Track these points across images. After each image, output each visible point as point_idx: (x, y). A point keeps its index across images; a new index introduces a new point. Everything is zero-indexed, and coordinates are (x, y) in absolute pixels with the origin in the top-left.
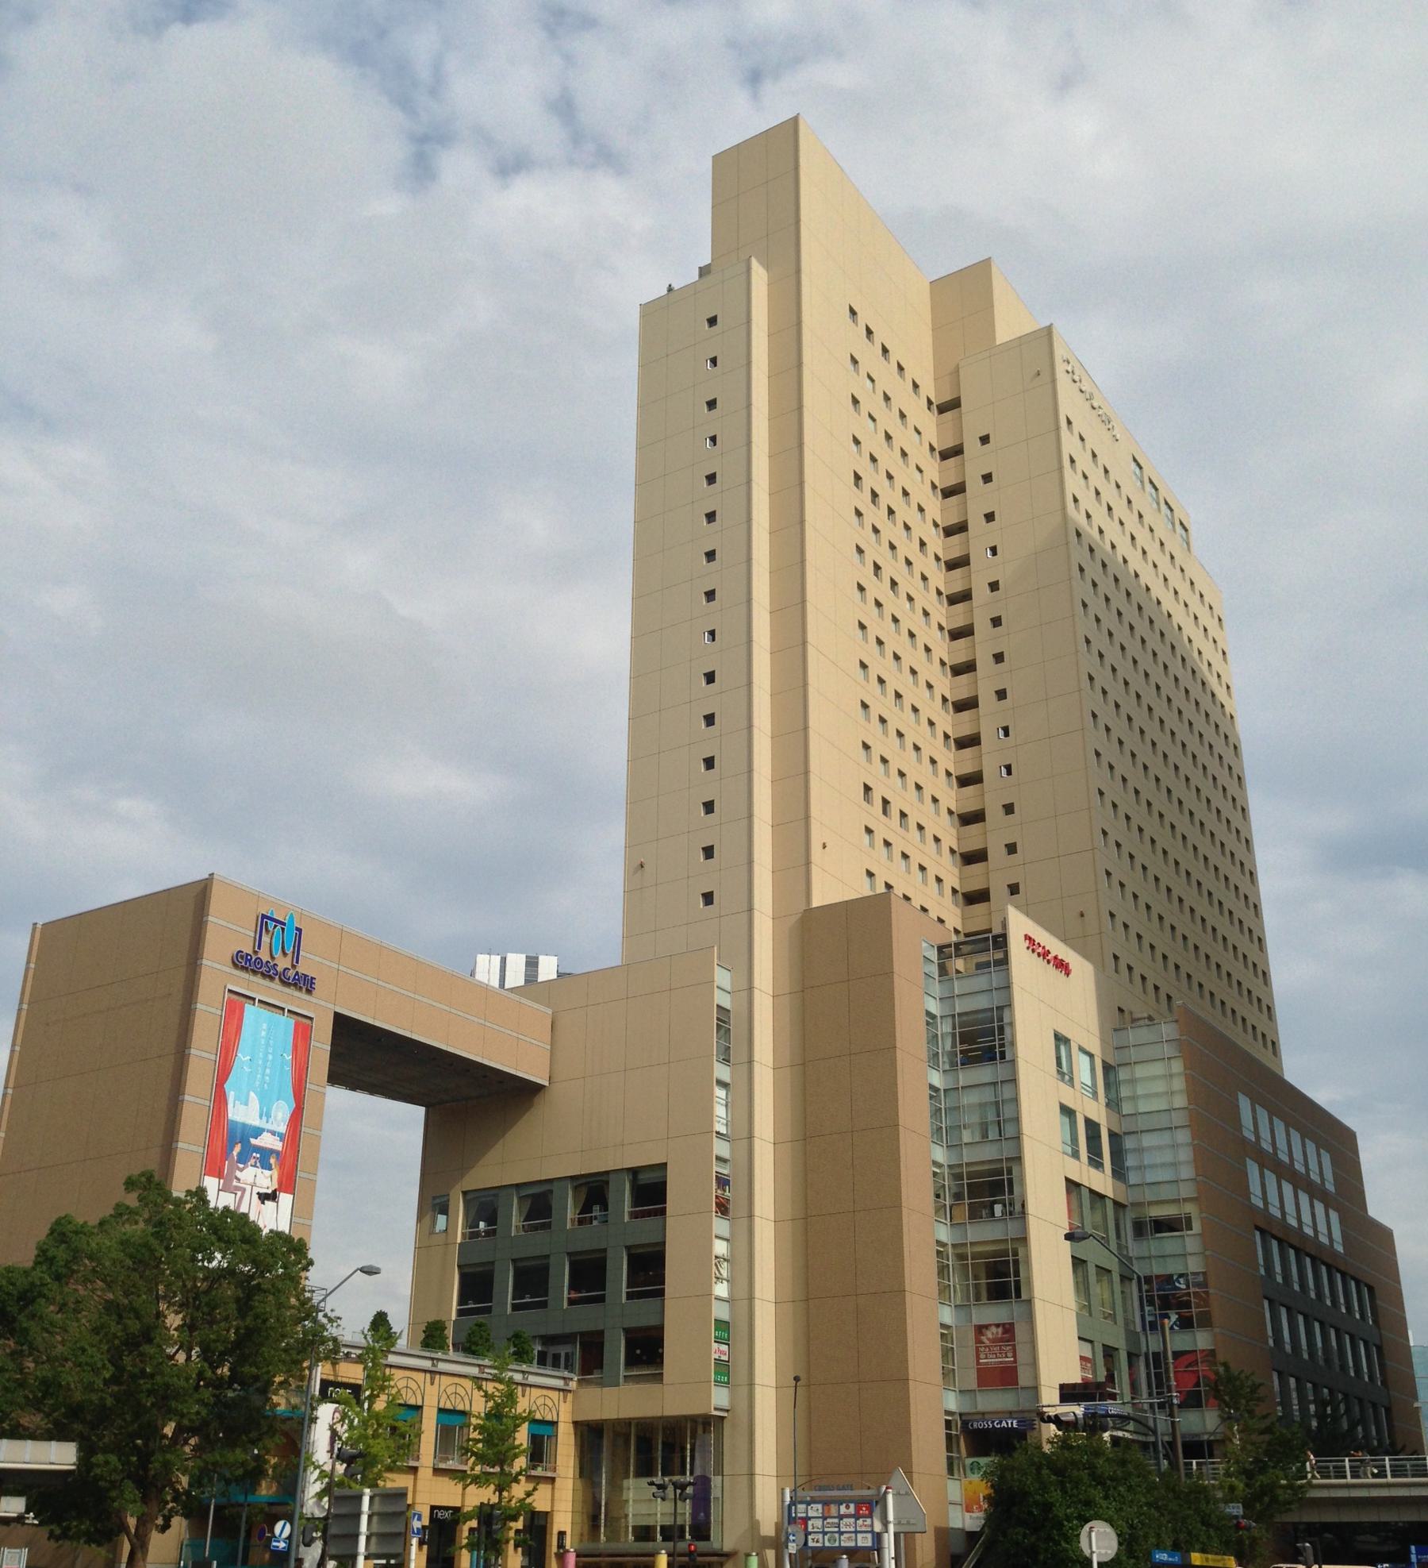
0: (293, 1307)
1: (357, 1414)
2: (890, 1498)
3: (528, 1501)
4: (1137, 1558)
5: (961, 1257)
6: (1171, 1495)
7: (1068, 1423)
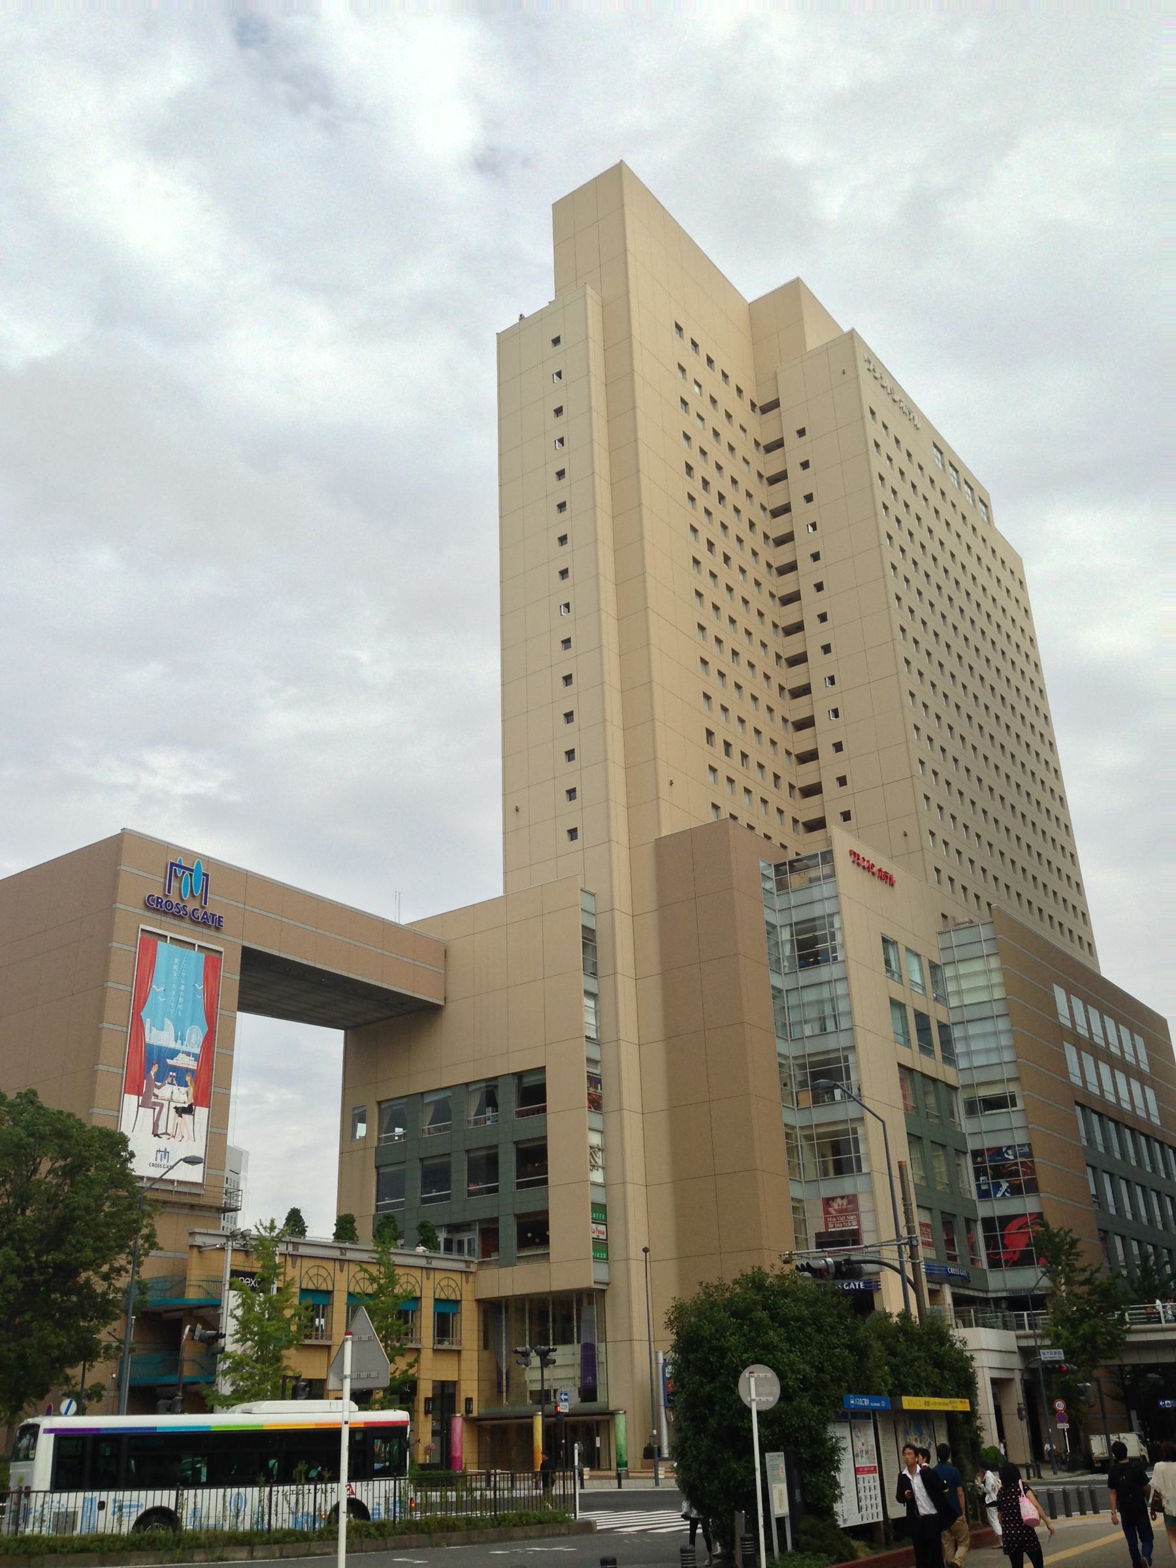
3: (411, 1372)
4: (822, 1404)
5: (809, 1138)
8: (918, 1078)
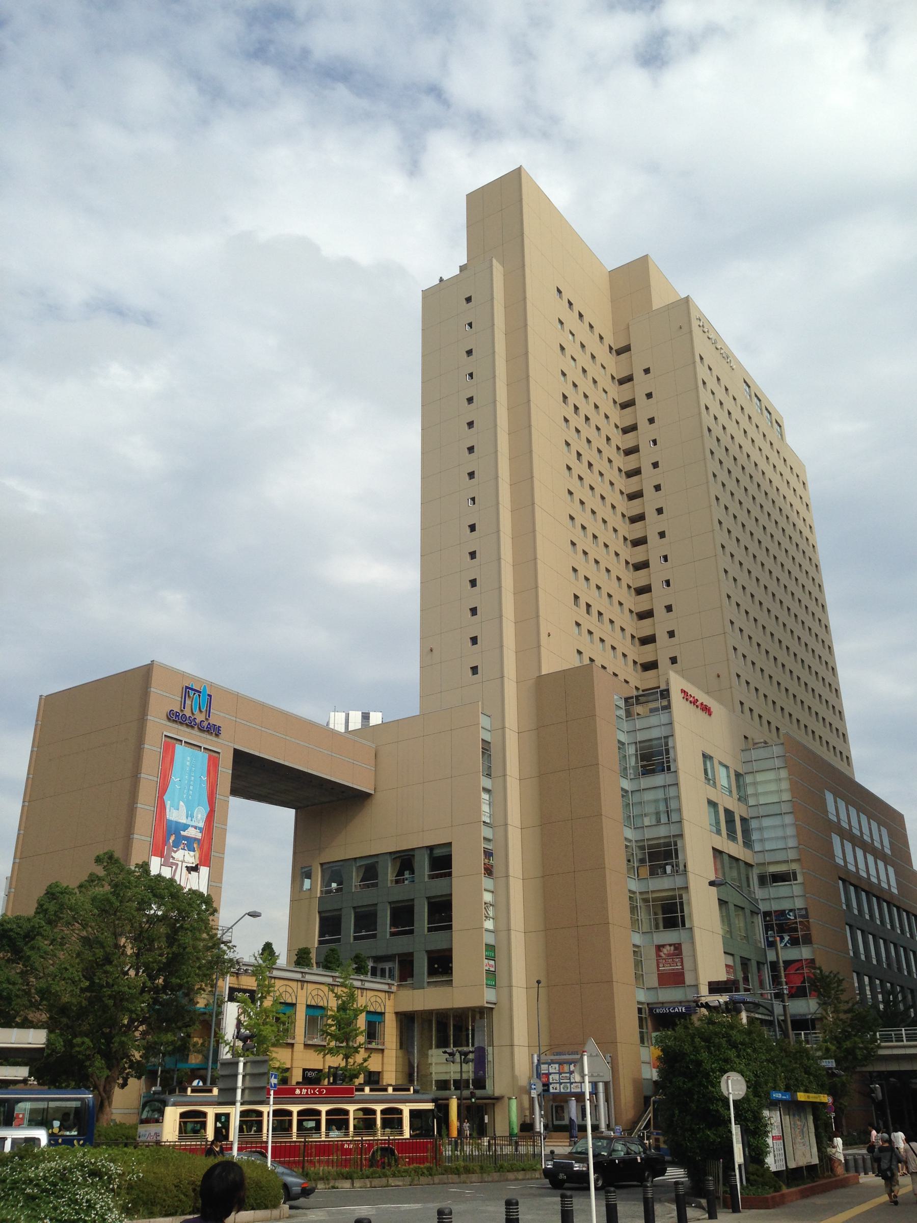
0: (204, 940)
1: (252, 1009)
2: (585, 1058)
3: (365, 1064)
4: (760, 1096)
5: (646, 901)
6: (783, 1054)
7: (715, 1008)
8: (726, 857)
